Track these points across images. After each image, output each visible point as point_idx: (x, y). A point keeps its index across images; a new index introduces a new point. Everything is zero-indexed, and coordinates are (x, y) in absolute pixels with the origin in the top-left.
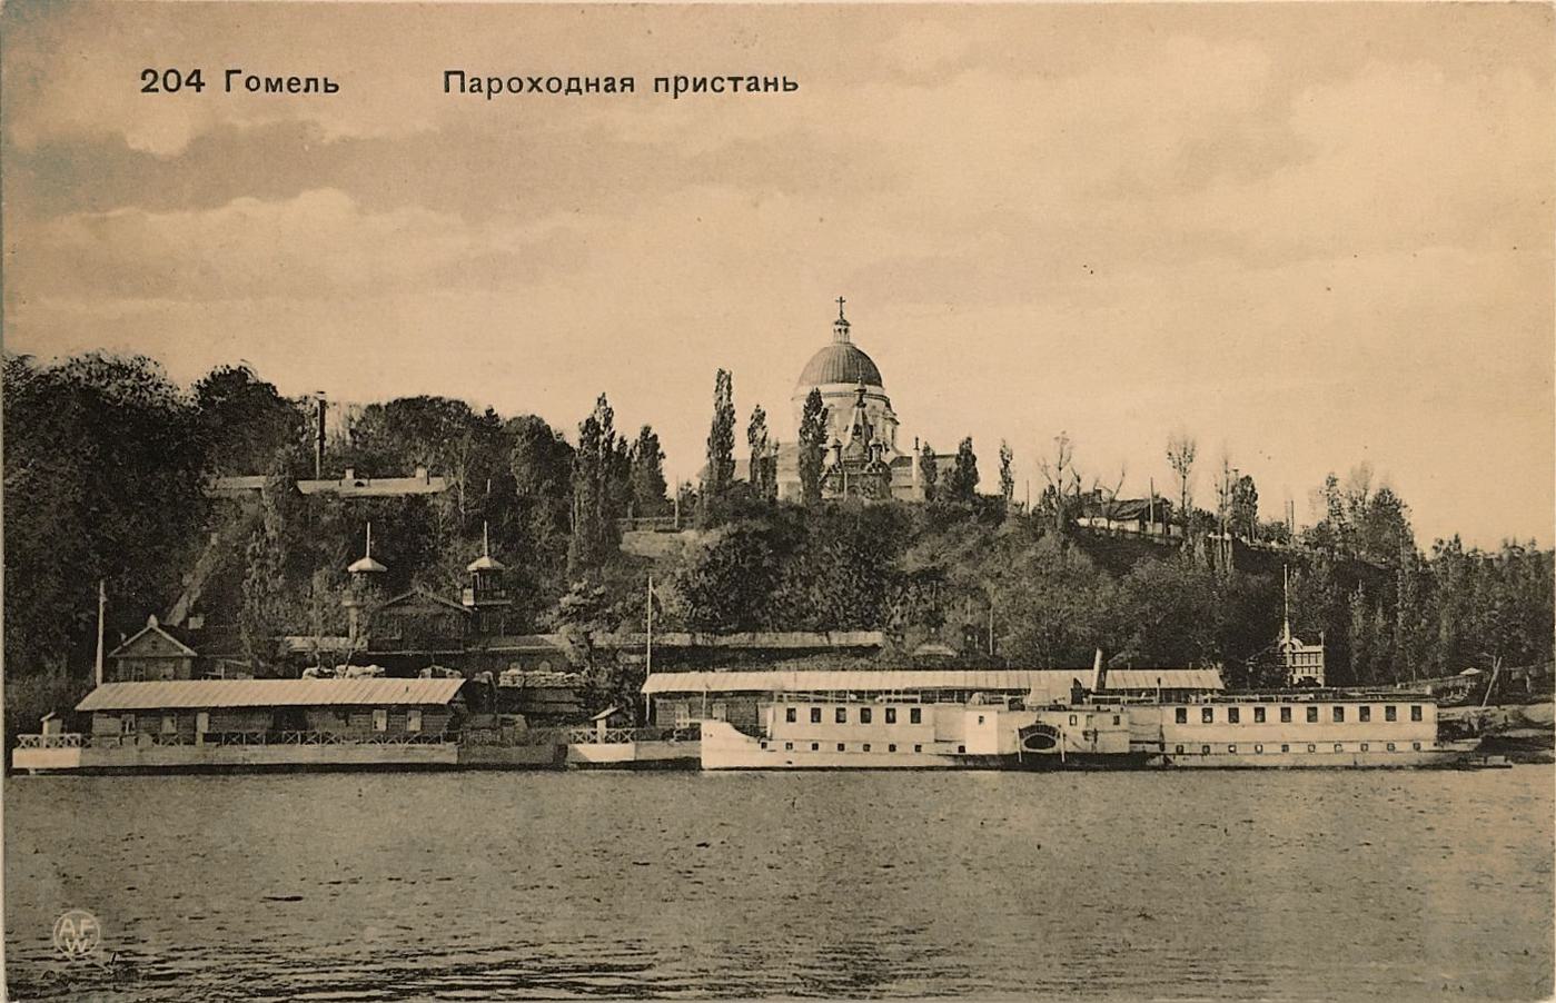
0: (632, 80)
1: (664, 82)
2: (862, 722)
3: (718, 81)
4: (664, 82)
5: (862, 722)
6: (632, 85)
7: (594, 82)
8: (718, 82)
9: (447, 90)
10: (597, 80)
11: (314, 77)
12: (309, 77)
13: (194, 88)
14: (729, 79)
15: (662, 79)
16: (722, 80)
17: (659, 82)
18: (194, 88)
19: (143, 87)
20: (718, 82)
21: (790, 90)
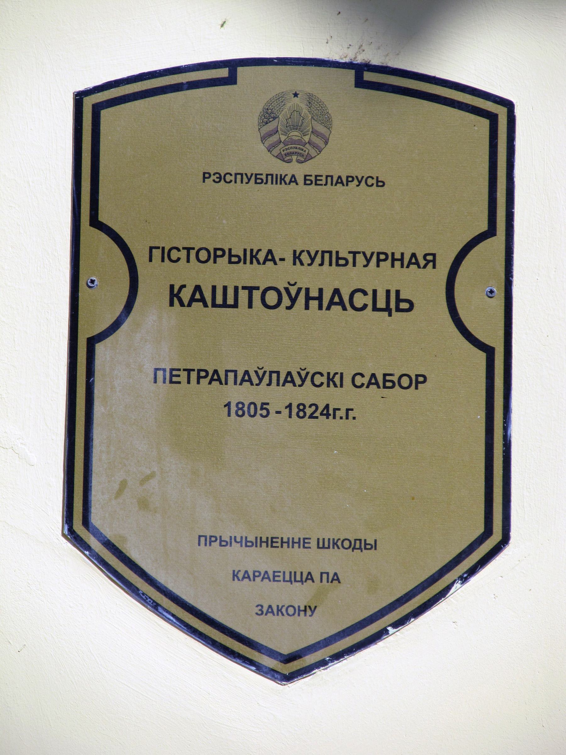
0: (434, 255)
1: (233, 374)
2: (235, 83)
3: (358, 295)
4: (233, 374)
5: (235, 83)
6: (434, 261)
7: (399, 257)
8: (174, 252)
9: (151, 260)
10: (198, 382)
11: (330, 174)
12: (201, 534)
13: (325, 417)
14: (184, 248)
15: (327, 252)
16: (179, 250)
17: (229, 374)
18: (325, 417)
19: (330, 406)
20: (174, 252)
21: (224, 546)
